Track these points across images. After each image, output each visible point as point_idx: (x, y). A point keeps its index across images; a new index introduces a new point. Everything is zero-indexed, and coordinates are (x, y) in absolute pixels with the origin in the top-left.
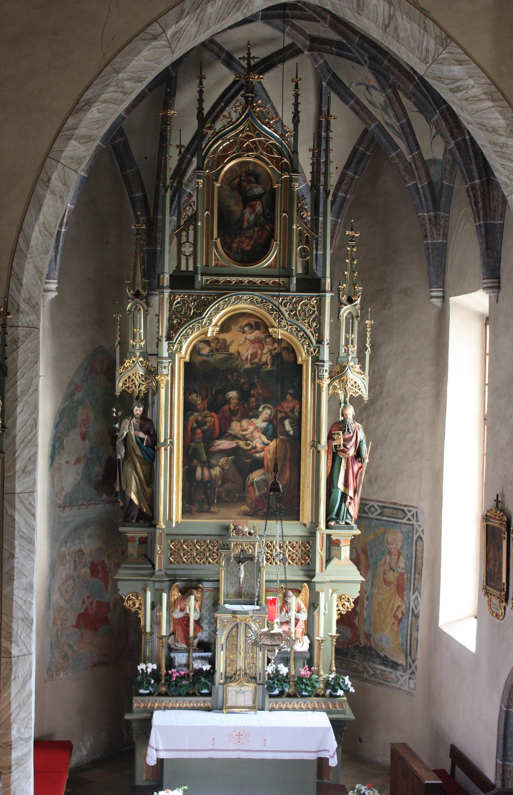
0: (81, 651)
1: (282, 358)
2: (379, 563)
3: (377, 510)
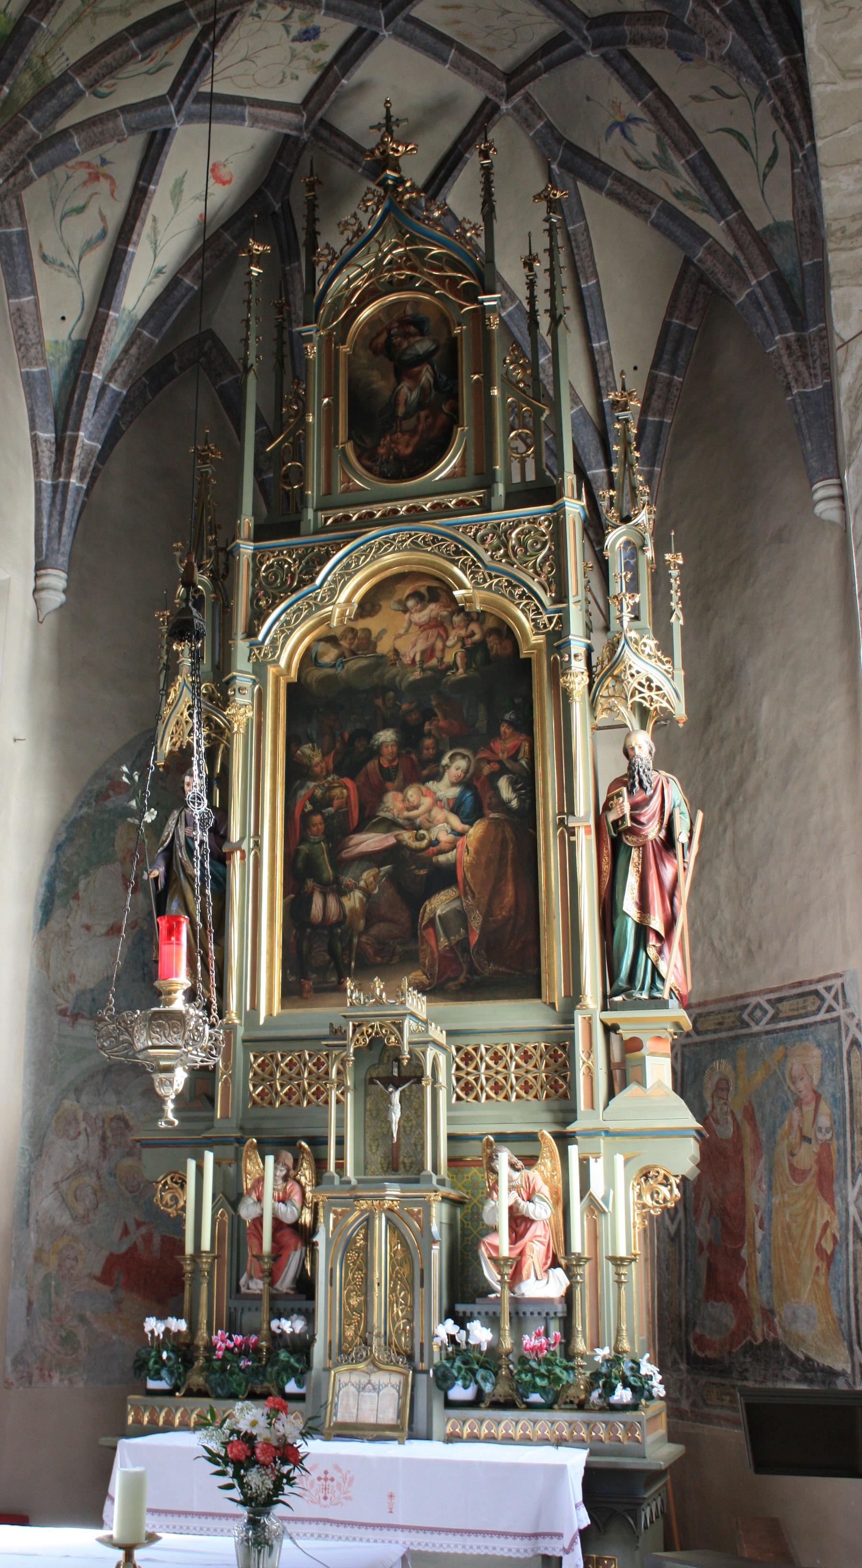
0: (114, 1337)
1: (487, 651)
2: (780, 1132)
3: (766, 1012)
